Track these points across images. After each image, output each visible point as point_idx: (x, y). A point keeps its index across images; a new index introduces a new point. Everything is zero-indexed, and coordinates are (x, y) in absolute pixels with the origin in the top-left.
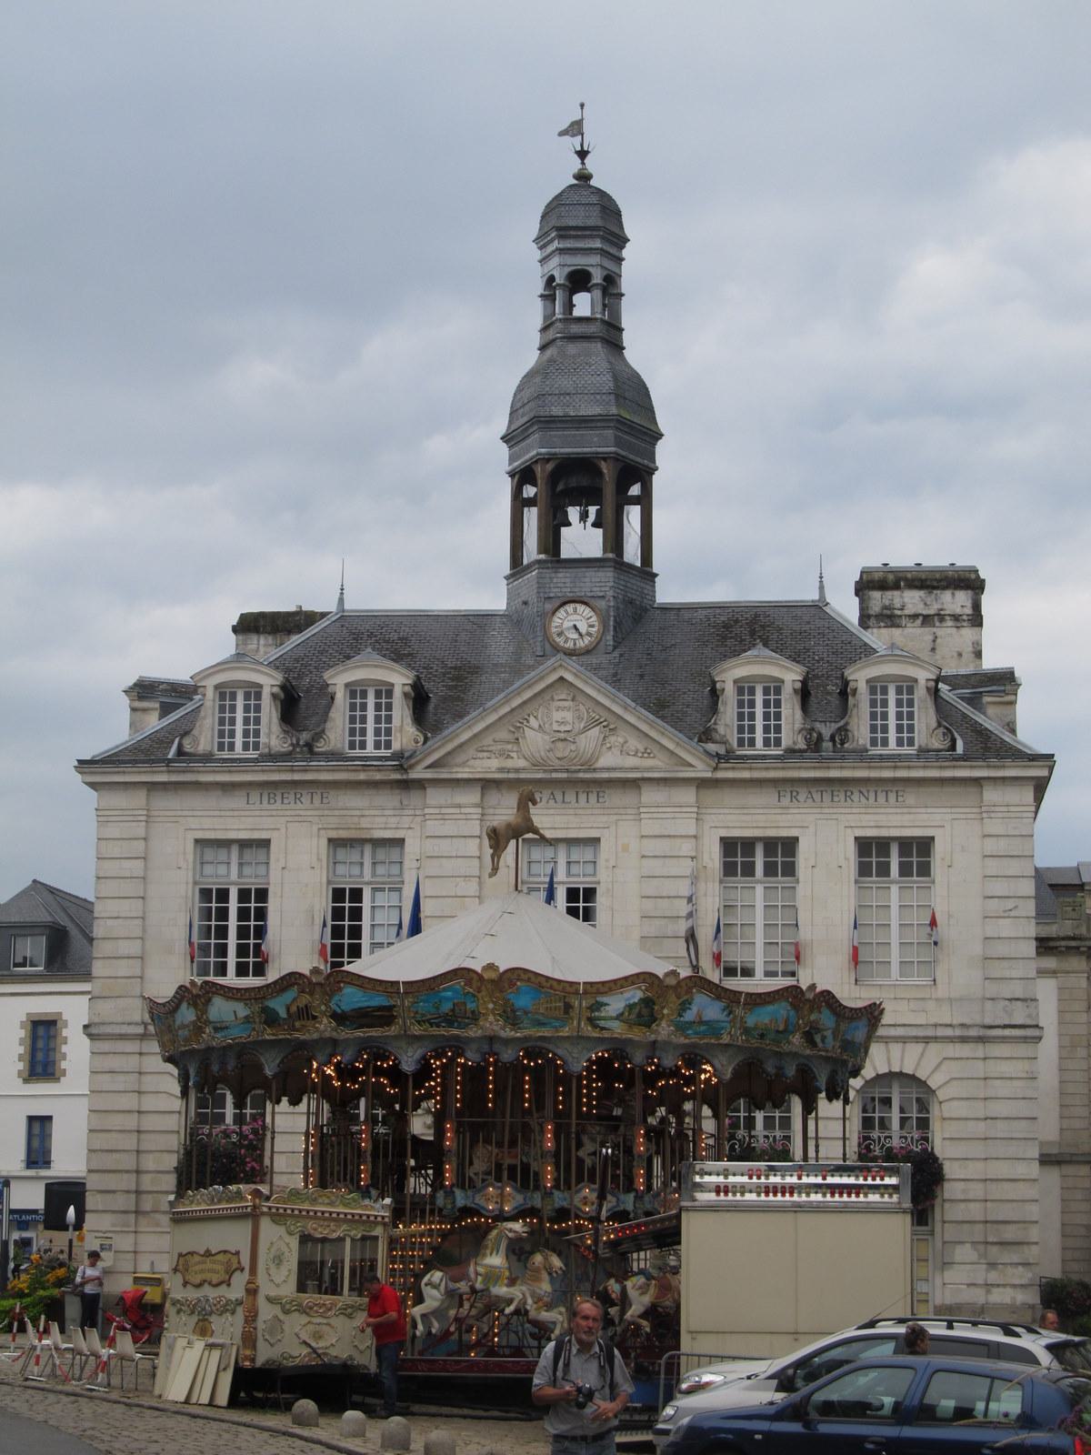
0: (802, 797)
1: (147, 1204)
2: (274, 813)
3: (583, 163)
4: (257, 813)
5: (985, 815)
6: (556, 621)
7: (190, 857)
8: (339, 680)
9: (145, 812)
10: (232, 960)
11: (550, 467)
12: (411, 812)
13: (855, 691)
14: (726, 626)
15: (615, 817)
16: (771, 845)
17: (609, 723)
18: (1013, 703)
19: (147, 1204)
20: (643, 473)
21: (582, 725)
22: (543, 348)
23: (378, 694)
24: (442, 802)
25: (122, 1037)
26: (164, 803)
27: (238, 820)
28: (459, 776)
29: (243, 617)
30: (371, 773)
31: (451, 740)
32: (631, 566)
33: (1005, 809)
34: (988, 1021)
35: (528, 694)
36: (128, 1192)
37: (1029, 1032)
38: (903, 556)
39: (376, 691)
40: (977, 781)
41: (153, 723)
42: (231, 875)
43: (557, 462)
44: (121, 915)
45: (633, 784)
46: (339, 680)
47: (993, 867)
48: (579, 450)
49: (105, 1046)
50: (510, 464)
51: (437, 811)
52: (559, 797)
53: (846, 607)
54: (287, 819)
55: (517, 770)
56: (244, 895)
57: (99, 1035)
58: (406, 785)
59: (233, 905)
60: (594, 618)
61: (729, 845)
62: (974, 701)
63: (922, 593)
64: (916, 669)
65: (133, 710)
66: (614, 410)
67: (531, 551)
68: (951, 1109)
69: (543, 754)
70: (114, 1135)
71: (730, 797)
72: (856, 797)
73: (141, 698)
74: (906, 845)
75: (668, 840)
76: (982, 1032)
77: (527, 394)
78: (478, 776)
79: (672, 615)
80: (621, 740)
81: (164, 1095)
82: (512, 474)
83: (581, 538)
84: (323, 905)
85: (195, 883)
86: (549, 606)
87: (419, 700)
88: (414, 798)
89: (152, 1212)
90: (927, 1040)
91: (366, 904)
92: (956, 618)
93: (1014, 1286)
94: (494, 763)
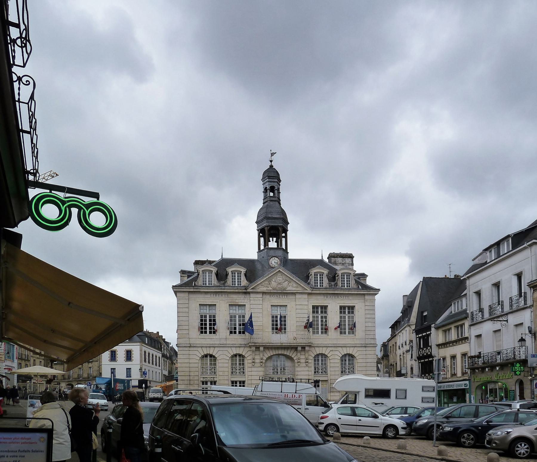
1: (192, 382)
2: (217, 299)
3: (271, 163)
4: (213, 298)
5: (365, 301)
6: (271, 261)
8: (230, 270)
11: (268, 228)
13: (338, 276)
16: (322, 307)
18: (366, 280)
19: (192, 382)
20: (285, 231)
21: (284, 281)
24: (254, 297)
26: (192, 296)
27: (208, 300)
28: (258, 291)
29: (196, 261)
31: (256, 283)
33: (369, 300)
34: (366, 343)
36: (188, 380)
37: (375, 345)
38: (337, 251)
40: (364, 294)
41: (186, 279)
42: (207, 311)
46: (230, 270)
47: (367, 312)
50: (257, 228)
52: (278, 296)
55: (270, 290)
58: (245, 293)
61: (314, 307)
62: (359, 278)
64: (351, 271)
65: (181, 276)
66: (282, 216)
67: (262, 247)
68: (359, 361)
71: (314, 297)
73: (183, 274)
74: (349, 307)
77: (262, 213)
78: (262, 291)
82: (258, 230)
83: (273, 244)
86: (269, 258)
88: (248, 296)
94: (265, 289)
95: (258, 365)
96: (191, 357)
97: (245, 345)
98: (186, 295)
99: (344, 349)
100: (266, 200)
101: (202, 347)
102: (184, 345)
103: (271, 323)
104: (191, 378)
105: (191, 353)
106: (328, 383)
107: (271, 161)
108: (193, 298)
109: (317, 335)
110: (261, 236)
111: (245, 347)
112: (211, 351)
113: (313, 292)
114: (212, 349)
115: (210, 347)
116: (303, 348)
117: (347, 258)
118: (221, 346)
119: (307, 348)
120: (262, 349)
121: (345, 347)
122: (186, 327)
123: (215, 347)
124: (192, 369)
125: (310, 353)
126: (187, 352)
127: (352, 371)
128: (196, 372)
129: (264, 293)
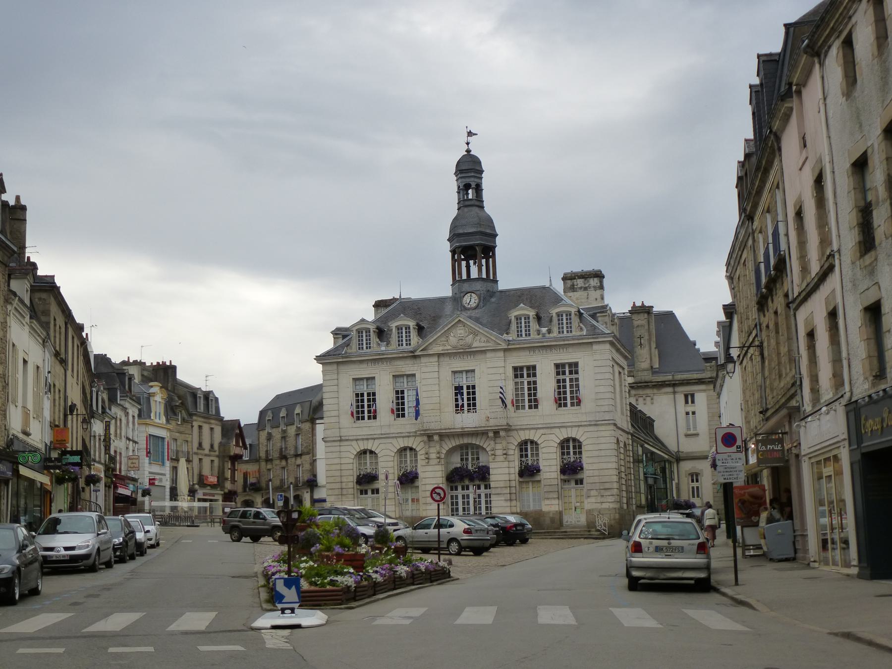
0: (537, 352)
1: (345, 492)
7: (351, 384)
8: (394, 325)
10: (568, 384)
11: (460, 249)
14: (520, 297)
17: (475, 334)
19: (345, 492)
22: (458, 209)
23: (406, 329)
25: (334, 441)
26: (343, 368)
27: (364, 371)
32: (484, 279)
34: (597, 419)
35: (450, 326)
40: (591, 343)
42: (364, 388)
45: (484, 352)
46: (394, 325)
49: (329, 444)
52: (462, 357)
53: (559, 287)
55: (447, 350)
56: (369, 394)
58: (415, 357)
59: (366, 398)
61: (515, 369)
63: (583, 280)
65: (334, 338)
71: (515, 354)
72: (553, 350)
76: (595, 423)
79: (503, 294)
80: (479, 338)
82: (451, 251)
84: (392, 396)
85: (354, 392)
86: (462, 295)
87: (420, 329)
88: (418, 361)
90: (579, 426)
91: (406, 395)
92: (594, 287)
93: (609, 502)
94: (441, 348)
96: (343, 455)
99: (563, 430)
100: (463, 204)
101: (357, 440)
103: (477, 396)
104: (344, 485)
105: (343, 449)
107: (468, 144)
109: (523, 411)
110: (463, 260)
111: (415, 436)
112: (369, 445)
113: (510, 347)
114: (371, 442)
115: (367, 439)
116: (496, 433)
117: (592, 279)
119: (502, 433)
120: (436, 438)
122: (335, 413)
123: (374, 439)
124: (344, 473)
125: (511, 440)
126: (337, 449)
129: (439, 355)
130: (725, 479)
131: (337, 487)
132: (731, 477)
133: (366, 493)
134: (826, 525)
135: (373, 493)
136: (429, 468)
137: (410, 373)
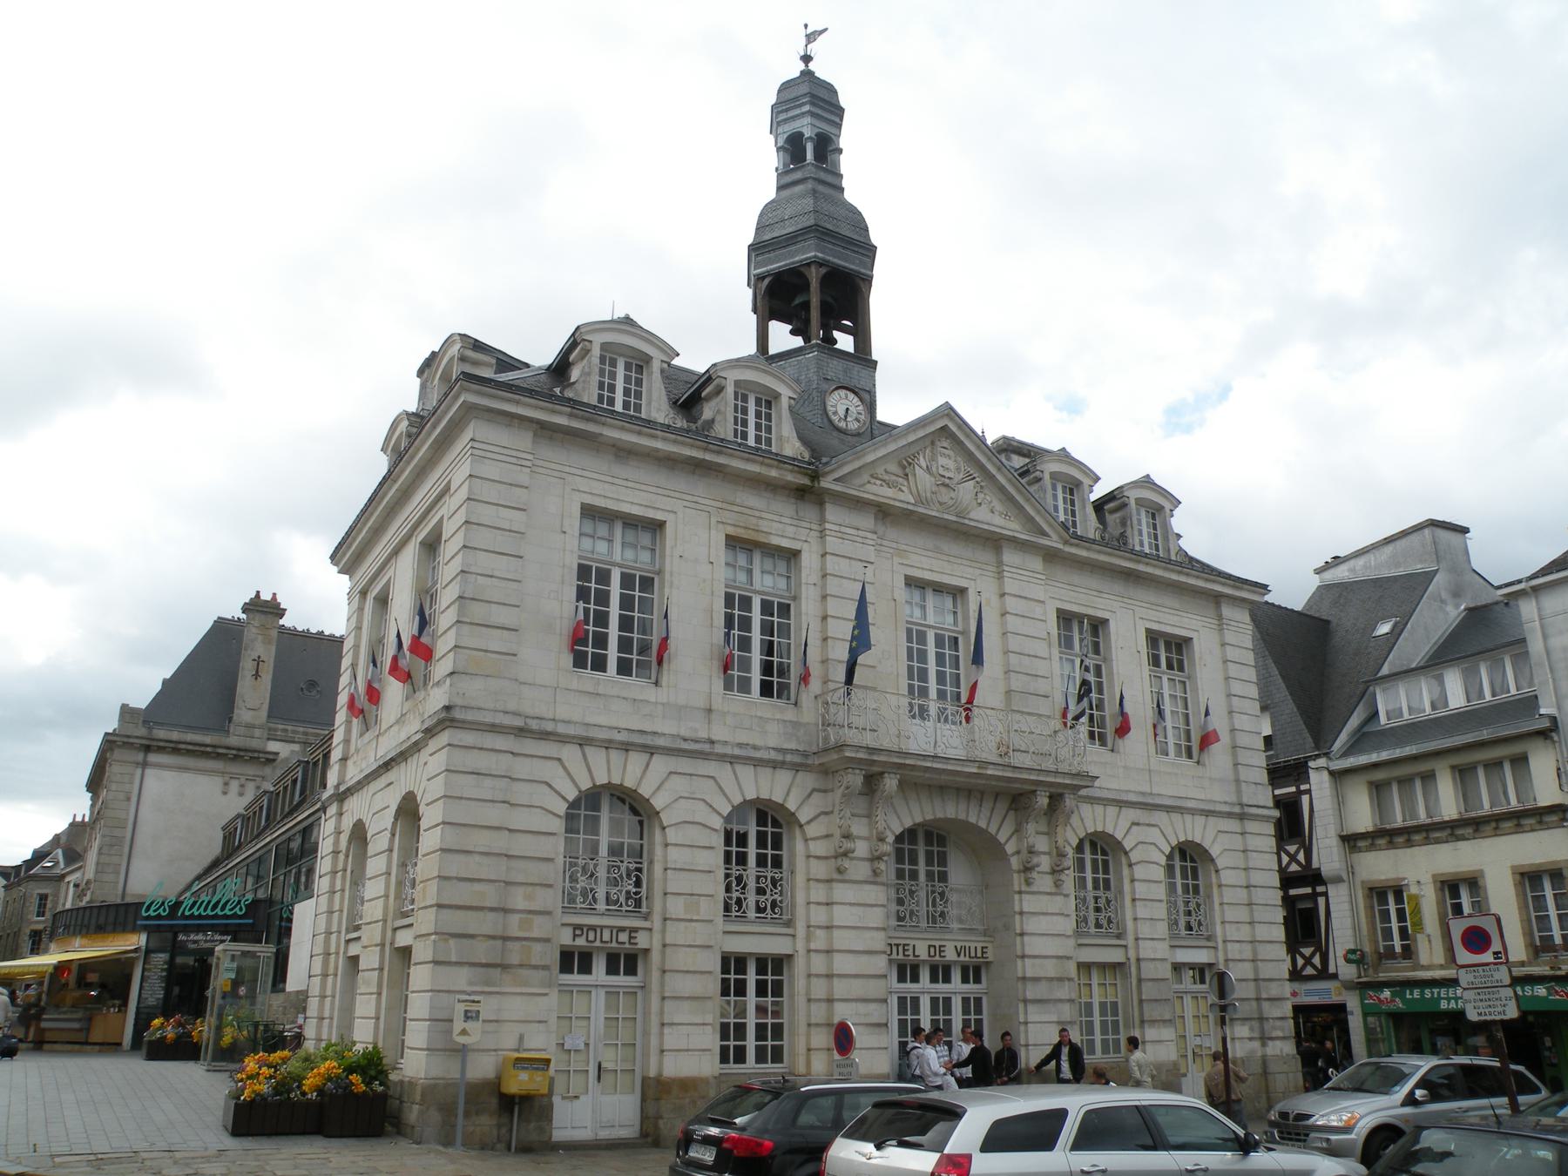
3: (807, 66)
5: (1225, 626)
9: (530, 457)
11: (823, 271)
12: (808, 525)
15: (979, 572)
24: (840, 521)
30: (782, 472)
39: (756, 398)
42: (617, 553)
43: (829, 269)
44: (497, 573)
48: (847, 265)
51: (837, 528)
54: (688, 504)
57: (464, 722)
60: (861, 408)
68: (676, 856)
69: (928, 495)
70: (477, 858)
75: (1024, 601)
81: (538, 810)
89: (521, 966)
95: (861, 870)
97: (805, 754)
98: (522, 440)
102: (488, 718)
105: (523, 768)
106: (1126, 976)
108: (553, 466)
112: (631, 772)
114: (636, 760)
115: (626, 747)
118: (685, 746)
121: (1179, 808)
123: (651, 750)
127: (627, 899)
128: (539, 891)
130: (1480, 1014)
131: (487, 929)
132: (1492, 1010)
133: (586, 968)
134: (521, 918)
135: (612, 969)
136: (842, 892)
137: (785, 543)
